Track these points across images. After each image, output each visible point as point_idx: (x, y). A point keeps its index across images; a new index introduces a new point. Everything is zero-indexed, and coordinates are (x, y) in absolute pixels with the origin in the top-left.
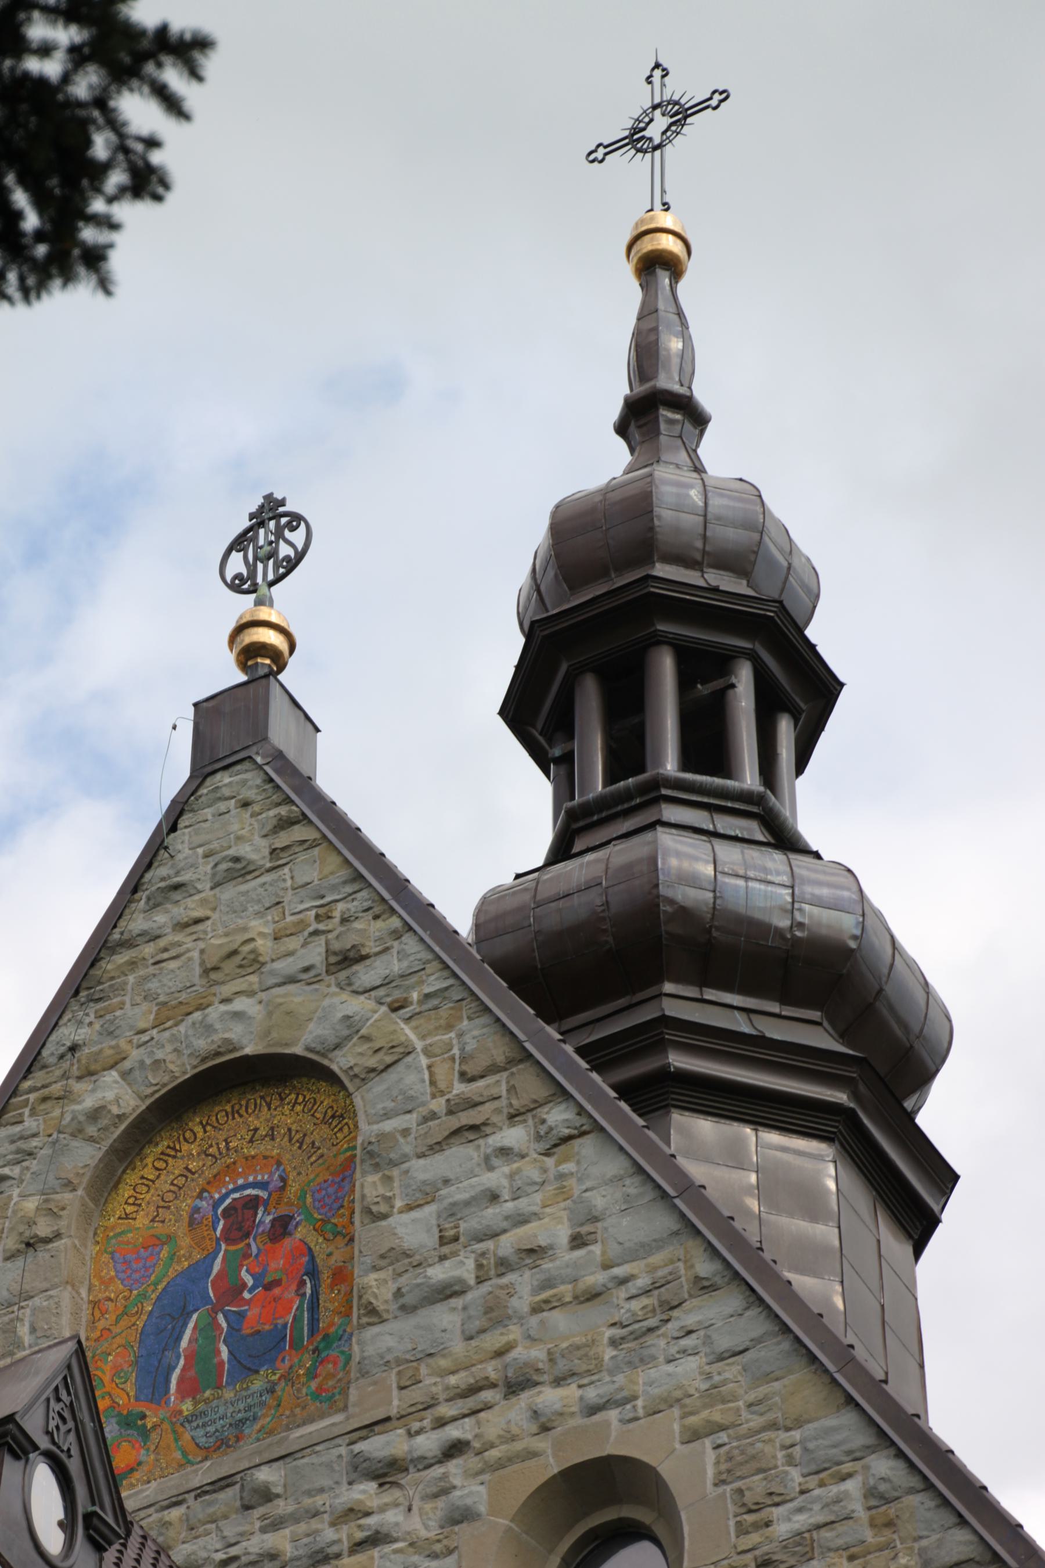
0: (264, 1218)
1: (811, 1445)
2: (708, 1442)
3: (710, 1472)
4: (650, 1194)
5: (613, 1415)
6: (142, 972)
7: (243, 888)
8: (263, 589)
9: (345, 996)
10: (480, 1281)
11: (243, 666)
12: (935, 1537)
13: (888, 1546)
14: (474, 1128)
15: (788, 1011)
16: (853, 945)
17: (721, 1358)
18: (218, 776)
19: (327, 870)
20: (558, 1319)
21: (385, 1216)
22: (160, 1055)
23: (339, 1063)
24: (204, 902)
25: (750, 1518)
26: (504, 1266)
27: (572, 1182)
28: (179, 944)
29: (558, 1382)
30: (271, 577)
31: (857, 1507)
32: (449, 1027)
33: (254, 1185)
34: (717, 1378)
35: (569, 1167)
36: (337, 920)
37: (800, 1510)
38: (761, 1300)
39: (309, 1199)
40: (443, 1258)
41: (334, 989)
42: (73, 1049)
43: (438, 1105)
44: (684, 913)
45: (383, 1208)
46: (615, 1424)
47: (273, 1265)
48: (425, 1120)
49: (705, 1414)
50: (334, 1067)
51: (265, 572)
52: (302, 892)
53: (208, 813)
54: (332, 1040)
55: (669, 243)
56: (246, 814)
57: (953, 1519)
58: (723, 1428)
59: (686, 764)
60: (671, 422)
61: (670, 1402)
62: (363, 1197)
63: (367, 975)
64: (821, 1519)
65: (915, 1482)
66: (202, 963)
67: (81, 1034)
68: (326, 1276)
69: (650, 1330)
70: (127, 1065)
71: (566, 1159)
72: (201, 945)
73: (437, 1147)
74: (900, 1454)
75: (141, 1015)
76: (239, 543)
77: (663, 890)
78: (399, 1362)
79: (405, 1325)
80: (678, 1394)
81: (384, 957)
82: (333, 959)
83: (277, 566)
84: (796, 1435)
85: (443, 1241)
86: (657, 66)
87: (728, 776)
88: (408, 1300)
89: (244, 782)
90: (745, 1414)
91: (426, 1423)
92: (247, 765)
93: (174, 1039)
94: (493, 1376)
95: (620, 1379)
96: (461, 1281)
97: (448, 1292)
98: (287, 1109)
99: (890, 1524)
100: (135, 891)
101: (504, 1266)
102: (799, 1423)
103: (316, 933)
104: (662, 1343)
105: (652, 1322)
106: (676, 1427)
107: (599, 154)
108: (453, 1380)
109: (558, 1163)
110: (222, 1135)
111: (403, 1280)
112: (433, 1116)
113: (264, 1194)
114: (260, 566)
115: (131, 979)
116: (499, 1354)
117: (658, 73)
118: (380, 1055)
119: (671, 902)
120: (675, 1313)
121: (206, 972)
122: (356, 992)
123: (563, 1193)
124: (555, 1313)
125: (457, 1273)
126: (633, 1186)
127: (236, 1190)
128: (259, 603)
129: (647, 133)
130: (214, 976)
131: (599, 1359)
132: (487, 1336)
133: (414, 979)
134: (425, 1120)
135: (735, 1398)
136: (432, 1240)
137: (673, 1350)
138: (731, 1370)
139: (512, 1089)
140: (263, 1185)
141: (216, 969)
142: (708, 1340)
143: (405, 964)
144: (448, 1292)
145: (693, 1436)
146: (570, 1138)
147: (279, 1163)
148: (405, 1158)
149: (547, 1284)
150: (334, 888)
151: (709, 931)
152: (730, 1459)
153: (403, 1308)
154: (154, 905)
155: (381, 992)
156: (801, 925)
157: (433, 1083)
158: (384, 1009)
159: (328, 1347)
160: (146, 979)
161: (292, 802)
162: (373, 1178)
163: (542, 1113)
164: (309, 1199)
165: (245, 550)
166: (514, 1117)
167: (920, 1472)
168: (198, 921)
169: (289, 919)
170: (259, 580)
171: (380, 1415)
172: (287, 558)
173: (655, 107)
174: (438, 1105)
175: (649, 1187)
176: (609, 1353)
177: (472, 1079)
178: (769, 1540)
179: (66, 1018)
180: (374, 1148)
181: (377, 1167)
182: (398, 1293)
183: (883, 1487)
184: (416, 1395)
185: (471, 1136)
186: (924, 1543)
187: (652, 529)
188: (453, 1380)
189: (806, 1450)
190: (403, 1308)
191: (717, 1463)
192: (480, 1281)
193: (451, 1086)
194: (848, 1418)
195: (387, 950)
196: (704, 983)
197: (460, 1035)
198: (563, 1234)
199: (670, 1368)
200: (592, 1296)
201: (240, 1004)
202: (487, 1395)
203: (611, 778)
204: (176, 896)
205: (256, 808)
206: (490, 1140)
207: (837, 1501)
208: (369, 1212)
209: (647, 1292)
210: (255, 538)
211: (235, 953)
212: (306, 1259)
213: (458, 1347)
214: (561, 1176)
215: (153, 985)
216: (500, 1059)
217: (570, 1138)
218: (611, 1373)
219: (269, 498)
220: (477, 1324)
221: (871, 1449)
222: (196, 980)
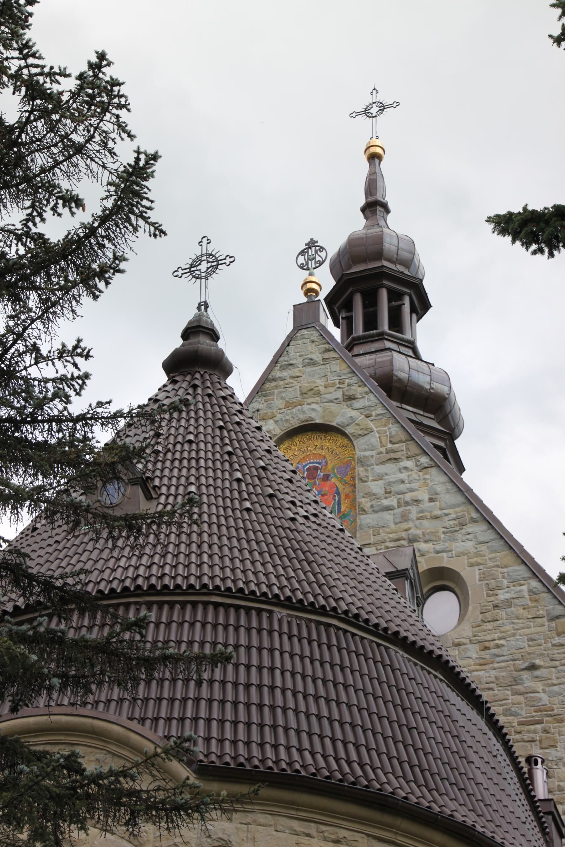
0: (321, 474)
1: (511, 574)
2: (476, 568)
3: (477, 577)
4: (455, 489)
5: (445, 555)
6: (280, 390)
7: (314, 369)
8: (312, 270)
9: (349, 410)
10: (399, 507)
11: (306, 294)
12: (551, 607)
13: (536, 607)
14: (395, 459)
15: (426, 414)
16: (447, 396)
17: (480, 543)
18: (303, 331)
19: (342, 368)
20: (426, 523)
21: (366, 482)
22: (287, 418)
23: (348, 430)
24: (300, 371)
25: (491, 592)
26: (407, 503)
27: (428, 481)
28: (292, 383)
29: (426, 542)
30: (314, 266)
31: (526, 594)
32: (385, 426)
33: (316, 463)
34: (479, 549)
35: (427, 476)
36: (346, 385)
37: (507, 592)
38: (493, 528)
39: (336, 471)
40: (386, 498)
41: (345, 407)
42: (258, 410)
43: (383, 450)
44: (400, 380)
45: (365, 479)
46: (445, 558)
47: (324, 489)
48: (379, 454)
49: (475, 559)
50: (347, 432)
51: (311, 264)
52: (334, 374)
53: (300, 342)
54: (346, 423)
55: (379, 150)
56: (314, 345)
57: (557, 602)
58: (481, 564)
59: (390, 328)
60: (380, 211)
61: (463, 554)
62: (359, 474)
63: (358, 404)
64: (514, 596)
65: (545, 590)
66: (300, 391)
67: (260, 406)
68: (343, 496)
69: (456, 531)
70: (276, 419)
71: (427, 474)
72: (300, 385)
73: (383, 463)
74: (540, 581)
75: (280, 404)
76: (302, 253)
77: (395, 372)
78: (373, 527)
79: (375, 516)
80: (466, 552)
81: (362, 400)
82: (345, 397)
83: (316, 263)
84: (505, 570)
85: (386, 492)
86: (375, 89)
87: (402, 333)
88: (375, 509)
89: (312, 334)
90: (488, 561)
91: (383, 547)
92: (313, 329)
93: (292, 413)
94: (404, 537)
95: (447, 544)
96: (393, 506)
97: (388, 509)
98: (327, 441)
99: (536, 601)
100: (276, 363)
101: (407, 503)
102: (506, 567)
103: (339, 388)
104: (460, 536)
105: (457, 529)
106: (466, 561)
107: (354, 115)
108: (391, 536)
109: (424, 475)
110: (305, 446)
111: (373, 502)
112: (381, 453)
113: (320, 466)
114: (310, 262)
115: (276, 391)
116: (406, 530)
117: (374, 92)
118: (363, 431)
119: (397, 376)
120: (464, 527)
121: (302, 394)
122: (353, 409)
123: (426, 484)
124: (424, 521)
125: (392, 503)
126: (449, 486)
127: (310, 463)
128: (311, 274)
129: (371, 111)
130: (305, 395)
131: (439, 538)
132: (402, 524)
133: (373, 408)
134: (379, 454)
135: (485, 556)
136: (382, 492)
137: (464, 538)
138: (484, 547)
139: (408, 449)
140: (320, 463)
141: (305, 393)
142: (475, 537)
143: (370, 403)
144: (388, 509)
145: (472, 565)
146: (428, 467)
147: (325, 457)
148: (372, 465)
149: (422, 512)
150: (344, 374)
151: (406, 387)
152: (484, 574)
153: (374, 511)
154: (283, 368)
155: (362, 411)
156: (433, 388)
157: (381, 442)
158: (363, 416)
159: (345, 517)
160: (281, 392)
161: (330, 344)
162: (361, 469)
163: (419, 458)
164: (336, 471)
165: (304, 255)
166: (408, 458)
167: (547, 587)
168: (298, 377)
169: (330, 382)
170: (310, 266)
171: (367, 542)
172: (319, 261)
173: (374, 103)
174: (383, 450)
175: (455, 487)
176: (443, 536)
177: (394, 444)
178: (497, 599)
179: (255, 400)
180: (362, 460)
181: (363, 466)
182: (372, 506)
183: (535, 590)
184: (379, 538)
185: (394, 461)
186: (548, 608)
187: (382, 249)
188: (391, 536)
189: (509, 575)
190: (374, 511)
191: (480, 574)
192: (399, 507)
193: (387, 444)
194: (522, 568)
195: (363, 397)
196: (401, 402)
197: (389, 429)
198: (426, 497)
199: (463, 543)
200: (436, 517)
201: (314, 406)
202: (402, 542)
203: (366, 329)
204: (290, 367)
205: (317, 344)
206: (401, 463)
207: (520, 591)
208: (361, 479)
209: (455, 519)
210: (308, 252)
211: (312, 389)
212: (335, 489)
213: (393, 526)
214: (425, 479)
215: (284, 395)
216: (403, 439)
217: (428, 467)
218: (443, 542)
219: (312, 239)
220: (398, 520)
221: (530, 578)
222: (298, 395)
